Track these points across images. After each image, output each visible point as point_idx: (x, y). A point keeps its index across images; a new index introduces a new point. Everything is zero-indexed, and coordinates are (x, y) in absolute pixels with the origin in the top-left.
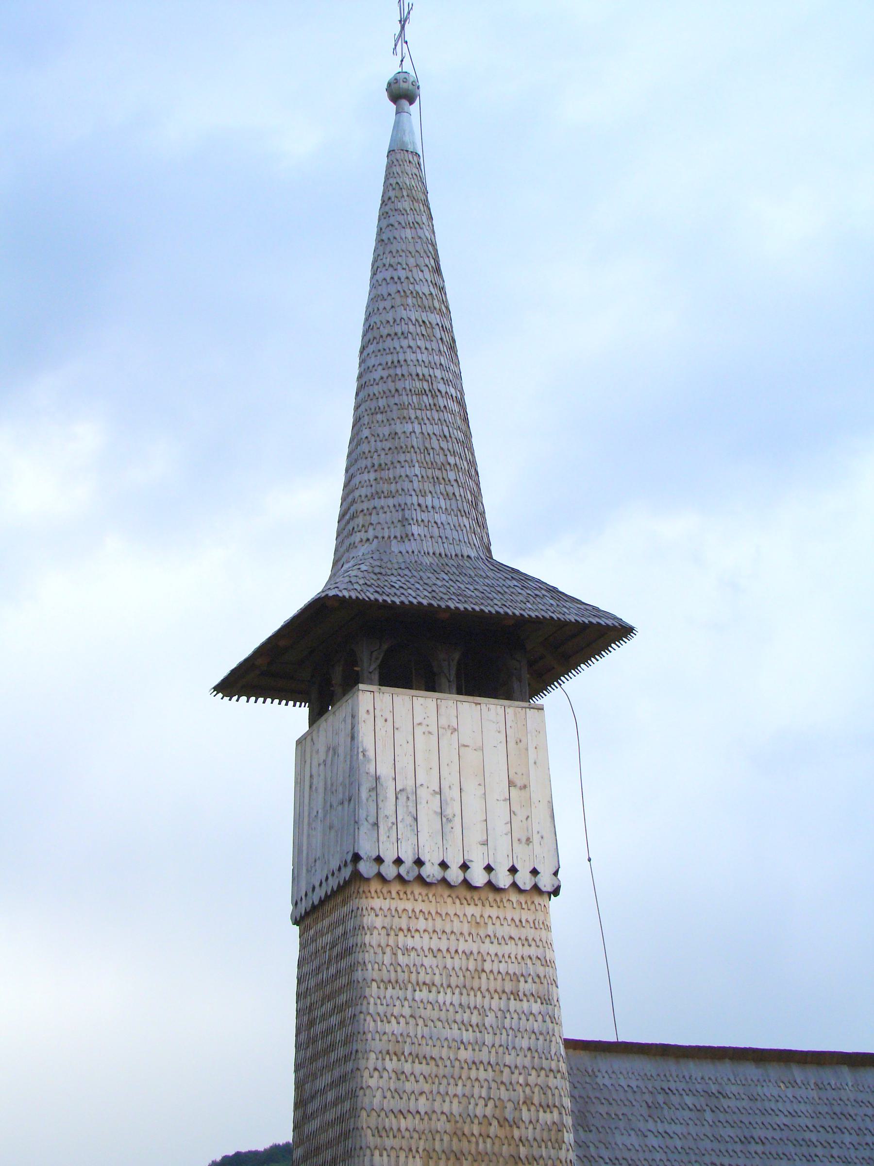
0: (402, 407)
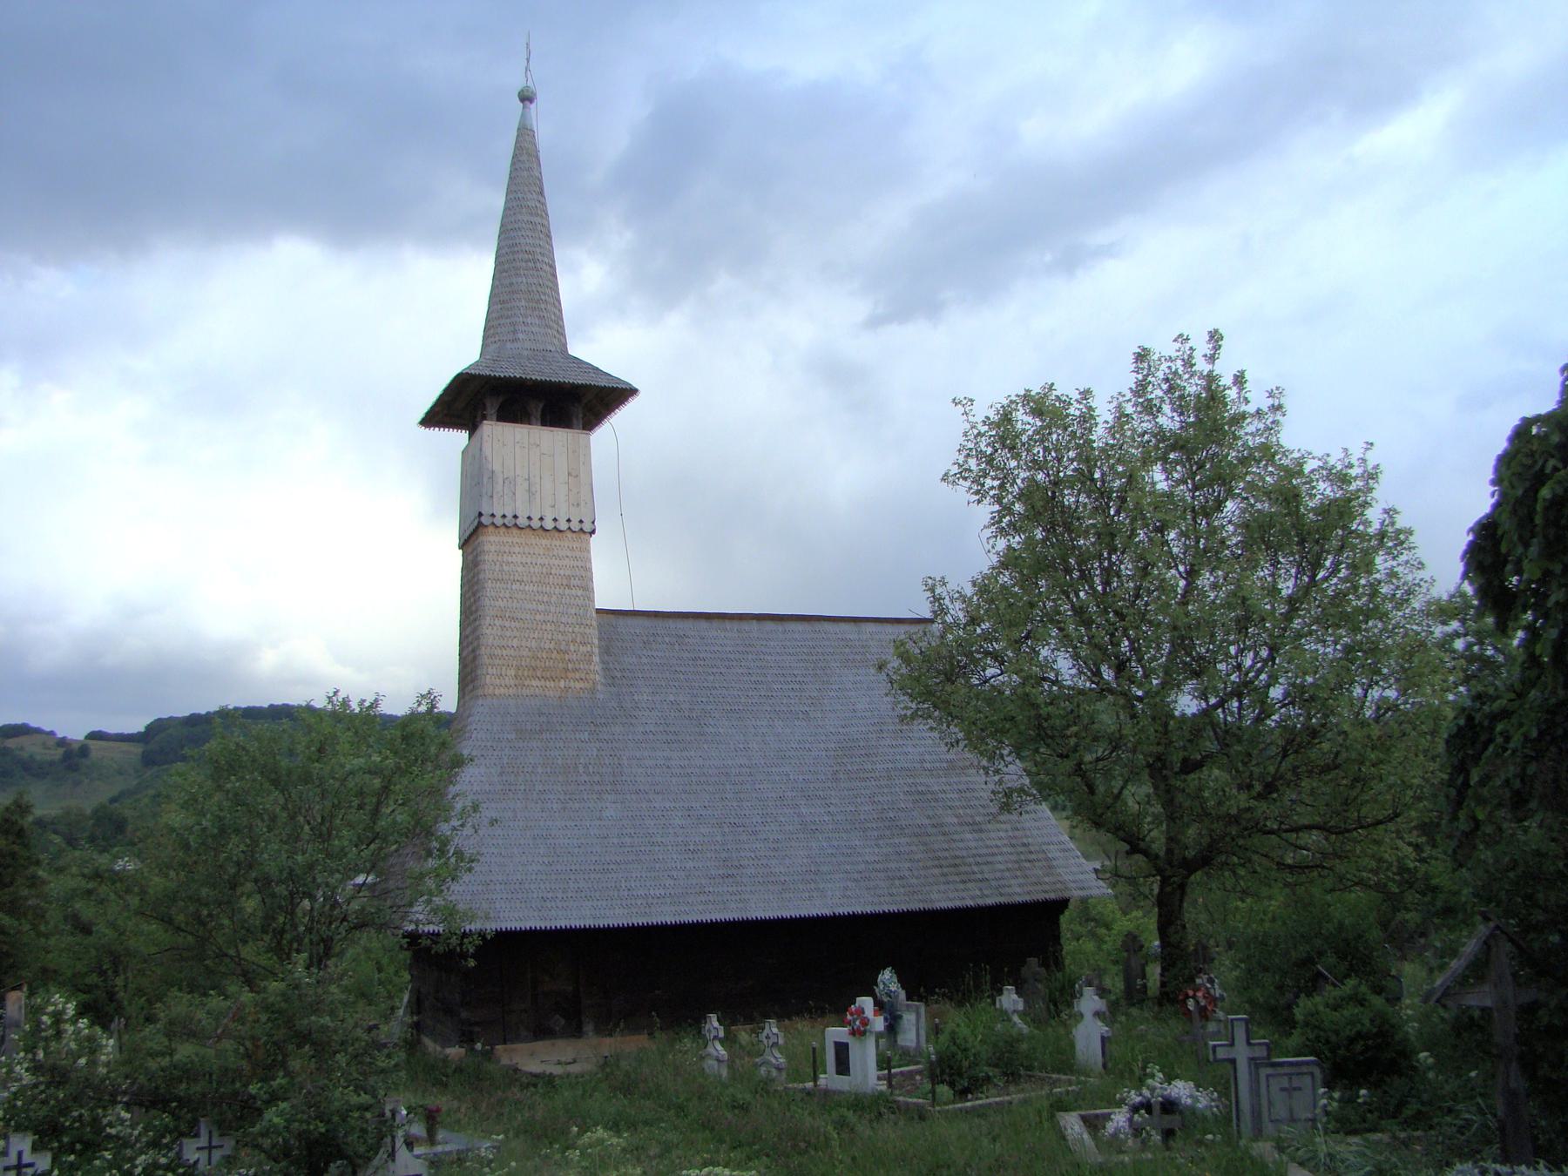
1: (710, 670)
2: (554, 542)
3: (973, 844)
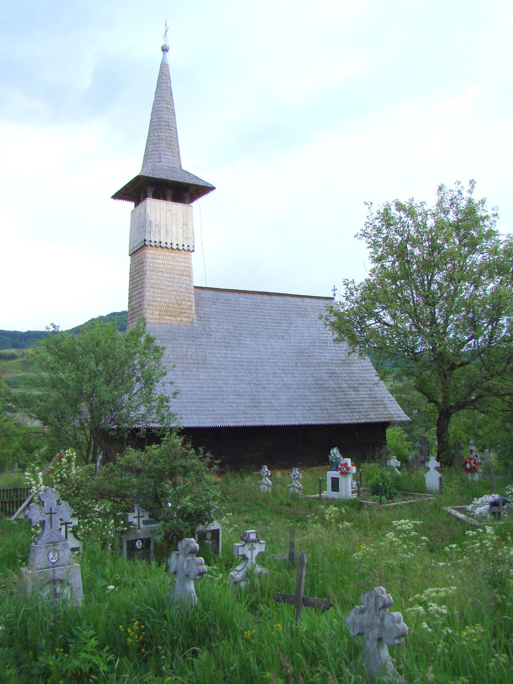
0: (161, 129)
1: (241, 316)
2: (177, 255)
3: (354, 396)
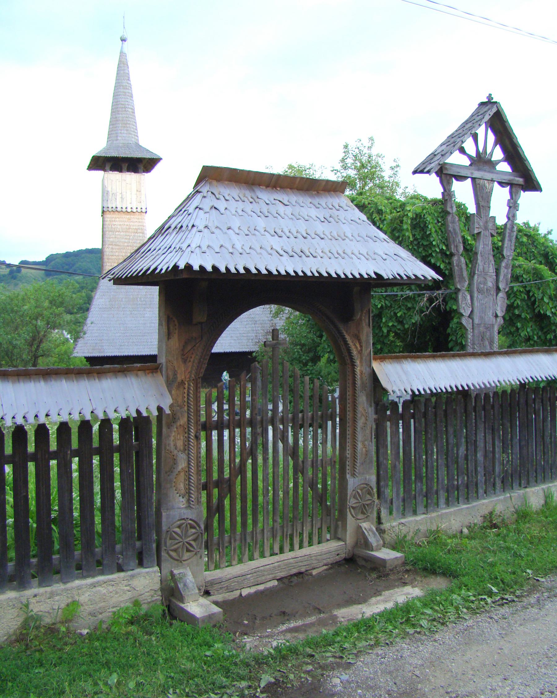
0: (118, 111)
